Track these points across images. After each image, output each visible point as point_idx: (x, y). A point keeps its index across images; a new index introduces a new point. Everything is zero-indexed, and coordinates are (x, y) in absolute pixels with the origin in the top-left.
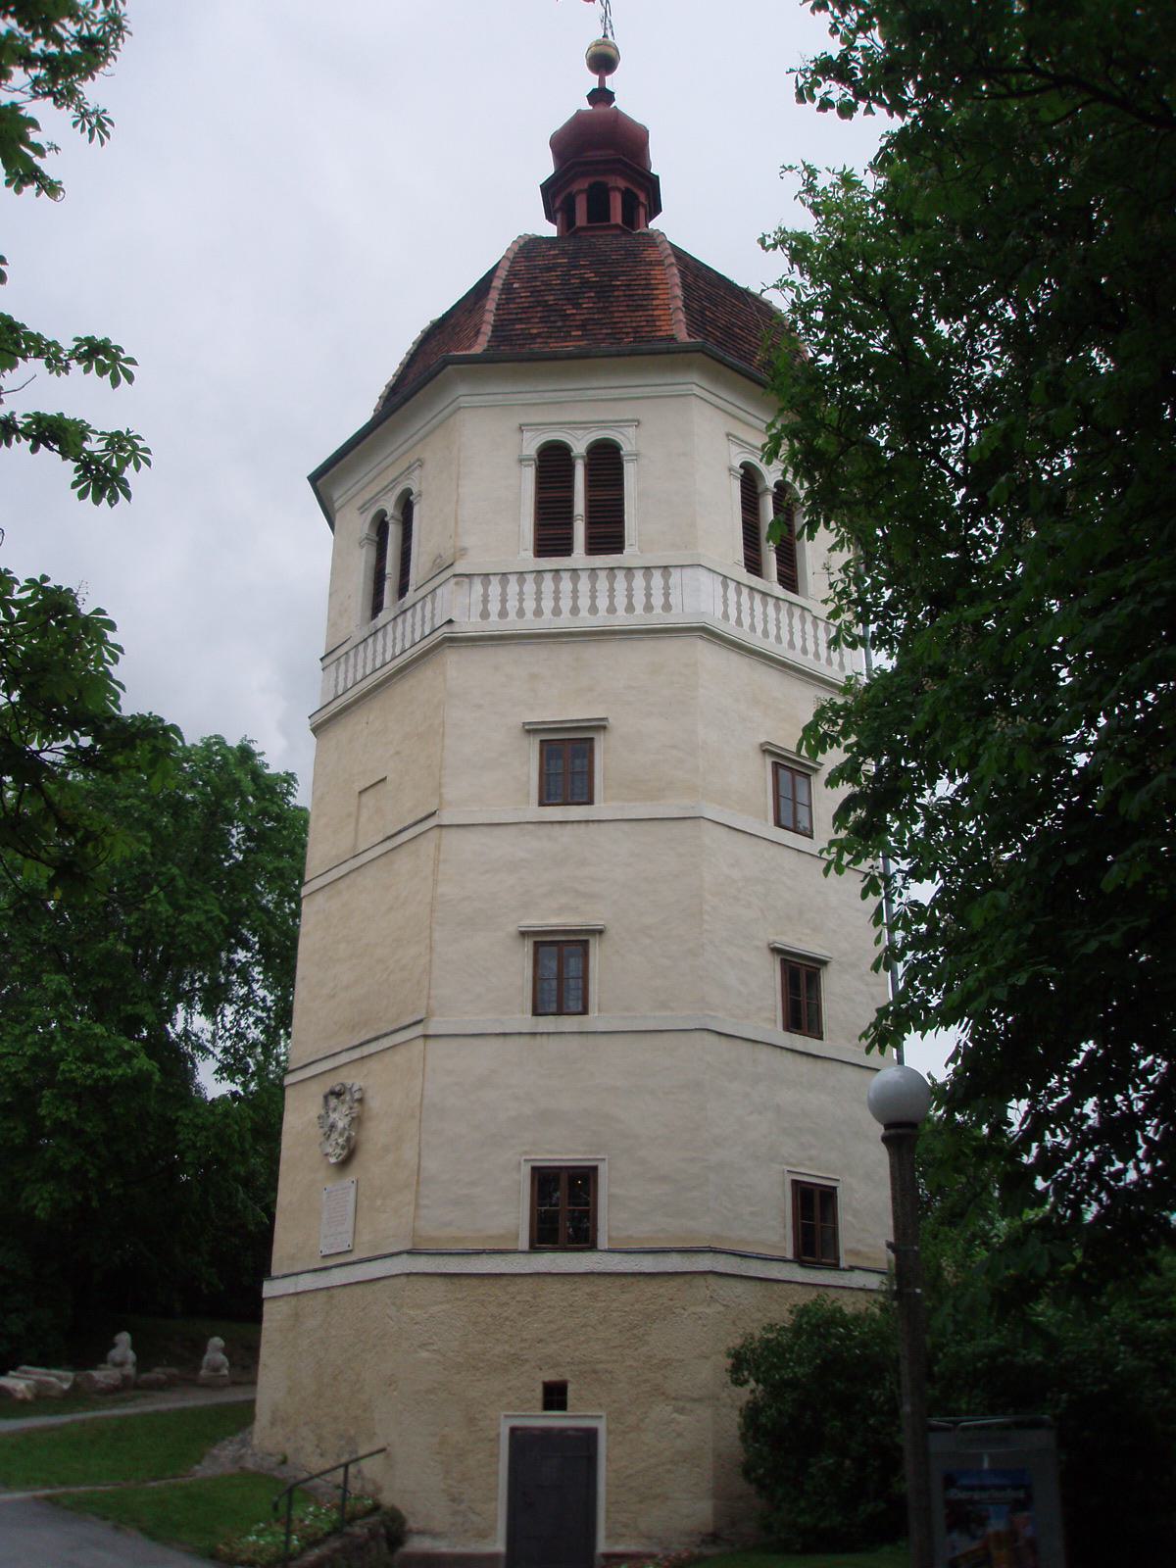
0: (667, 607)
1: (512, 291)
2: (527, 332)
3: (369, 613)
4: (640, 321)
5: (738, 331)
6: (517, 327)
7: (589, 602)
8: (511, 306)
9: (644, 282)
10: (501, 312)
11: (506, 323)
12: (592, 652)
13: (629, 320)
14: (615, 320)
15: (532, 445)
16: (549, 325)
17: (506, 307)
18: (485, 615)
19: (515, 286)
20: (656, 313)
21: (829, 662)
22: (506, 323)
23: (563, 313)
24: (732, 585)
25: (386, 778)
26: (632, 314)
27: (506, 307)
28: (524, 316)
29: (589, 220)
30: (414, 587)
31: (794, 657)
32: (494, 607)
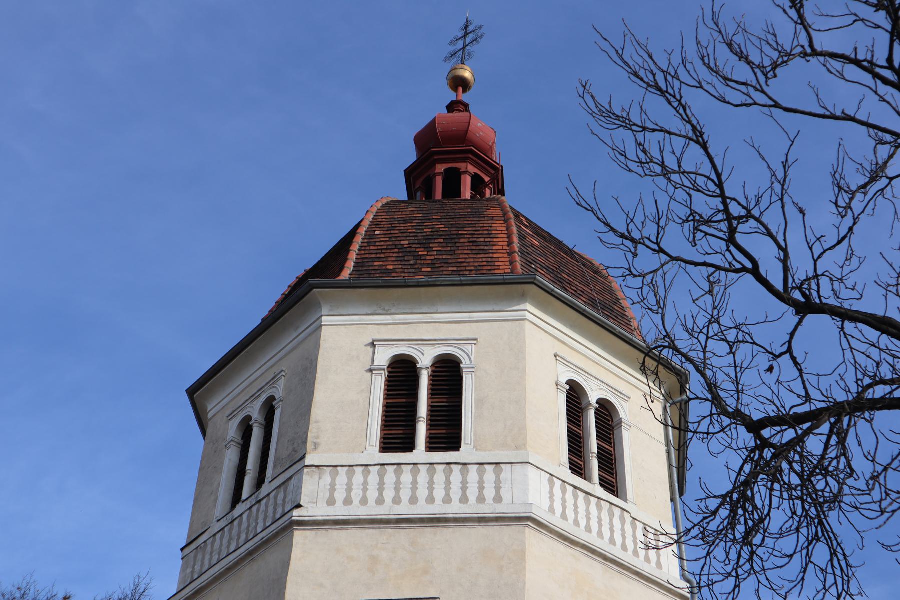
0: (498, 499)
1: (375, 237)
2: (384, 268)
3: (229, 506)
4: (482, 262)
5: (566, 277)
6: (376, 264)
8: (372, 248)
9: (486, 232)
10: (363, 252)
11: (366, 261)
12: (428, 535)
13: (472, 260)
14: (460, 261)
15: (383, 357)
16: (404, 263)
17: (368, 248)
18: (331, 502)
19: (377, 233)
20: (495, 256)
21: (647, 559)
22: (366, 261)
23: (416, 254)
24: (558, 483)
26: (475, 257)
27: (368, 248)
28: (382, 256)
29: (443, 197)
31: (616, 552)
32: (340, 496)
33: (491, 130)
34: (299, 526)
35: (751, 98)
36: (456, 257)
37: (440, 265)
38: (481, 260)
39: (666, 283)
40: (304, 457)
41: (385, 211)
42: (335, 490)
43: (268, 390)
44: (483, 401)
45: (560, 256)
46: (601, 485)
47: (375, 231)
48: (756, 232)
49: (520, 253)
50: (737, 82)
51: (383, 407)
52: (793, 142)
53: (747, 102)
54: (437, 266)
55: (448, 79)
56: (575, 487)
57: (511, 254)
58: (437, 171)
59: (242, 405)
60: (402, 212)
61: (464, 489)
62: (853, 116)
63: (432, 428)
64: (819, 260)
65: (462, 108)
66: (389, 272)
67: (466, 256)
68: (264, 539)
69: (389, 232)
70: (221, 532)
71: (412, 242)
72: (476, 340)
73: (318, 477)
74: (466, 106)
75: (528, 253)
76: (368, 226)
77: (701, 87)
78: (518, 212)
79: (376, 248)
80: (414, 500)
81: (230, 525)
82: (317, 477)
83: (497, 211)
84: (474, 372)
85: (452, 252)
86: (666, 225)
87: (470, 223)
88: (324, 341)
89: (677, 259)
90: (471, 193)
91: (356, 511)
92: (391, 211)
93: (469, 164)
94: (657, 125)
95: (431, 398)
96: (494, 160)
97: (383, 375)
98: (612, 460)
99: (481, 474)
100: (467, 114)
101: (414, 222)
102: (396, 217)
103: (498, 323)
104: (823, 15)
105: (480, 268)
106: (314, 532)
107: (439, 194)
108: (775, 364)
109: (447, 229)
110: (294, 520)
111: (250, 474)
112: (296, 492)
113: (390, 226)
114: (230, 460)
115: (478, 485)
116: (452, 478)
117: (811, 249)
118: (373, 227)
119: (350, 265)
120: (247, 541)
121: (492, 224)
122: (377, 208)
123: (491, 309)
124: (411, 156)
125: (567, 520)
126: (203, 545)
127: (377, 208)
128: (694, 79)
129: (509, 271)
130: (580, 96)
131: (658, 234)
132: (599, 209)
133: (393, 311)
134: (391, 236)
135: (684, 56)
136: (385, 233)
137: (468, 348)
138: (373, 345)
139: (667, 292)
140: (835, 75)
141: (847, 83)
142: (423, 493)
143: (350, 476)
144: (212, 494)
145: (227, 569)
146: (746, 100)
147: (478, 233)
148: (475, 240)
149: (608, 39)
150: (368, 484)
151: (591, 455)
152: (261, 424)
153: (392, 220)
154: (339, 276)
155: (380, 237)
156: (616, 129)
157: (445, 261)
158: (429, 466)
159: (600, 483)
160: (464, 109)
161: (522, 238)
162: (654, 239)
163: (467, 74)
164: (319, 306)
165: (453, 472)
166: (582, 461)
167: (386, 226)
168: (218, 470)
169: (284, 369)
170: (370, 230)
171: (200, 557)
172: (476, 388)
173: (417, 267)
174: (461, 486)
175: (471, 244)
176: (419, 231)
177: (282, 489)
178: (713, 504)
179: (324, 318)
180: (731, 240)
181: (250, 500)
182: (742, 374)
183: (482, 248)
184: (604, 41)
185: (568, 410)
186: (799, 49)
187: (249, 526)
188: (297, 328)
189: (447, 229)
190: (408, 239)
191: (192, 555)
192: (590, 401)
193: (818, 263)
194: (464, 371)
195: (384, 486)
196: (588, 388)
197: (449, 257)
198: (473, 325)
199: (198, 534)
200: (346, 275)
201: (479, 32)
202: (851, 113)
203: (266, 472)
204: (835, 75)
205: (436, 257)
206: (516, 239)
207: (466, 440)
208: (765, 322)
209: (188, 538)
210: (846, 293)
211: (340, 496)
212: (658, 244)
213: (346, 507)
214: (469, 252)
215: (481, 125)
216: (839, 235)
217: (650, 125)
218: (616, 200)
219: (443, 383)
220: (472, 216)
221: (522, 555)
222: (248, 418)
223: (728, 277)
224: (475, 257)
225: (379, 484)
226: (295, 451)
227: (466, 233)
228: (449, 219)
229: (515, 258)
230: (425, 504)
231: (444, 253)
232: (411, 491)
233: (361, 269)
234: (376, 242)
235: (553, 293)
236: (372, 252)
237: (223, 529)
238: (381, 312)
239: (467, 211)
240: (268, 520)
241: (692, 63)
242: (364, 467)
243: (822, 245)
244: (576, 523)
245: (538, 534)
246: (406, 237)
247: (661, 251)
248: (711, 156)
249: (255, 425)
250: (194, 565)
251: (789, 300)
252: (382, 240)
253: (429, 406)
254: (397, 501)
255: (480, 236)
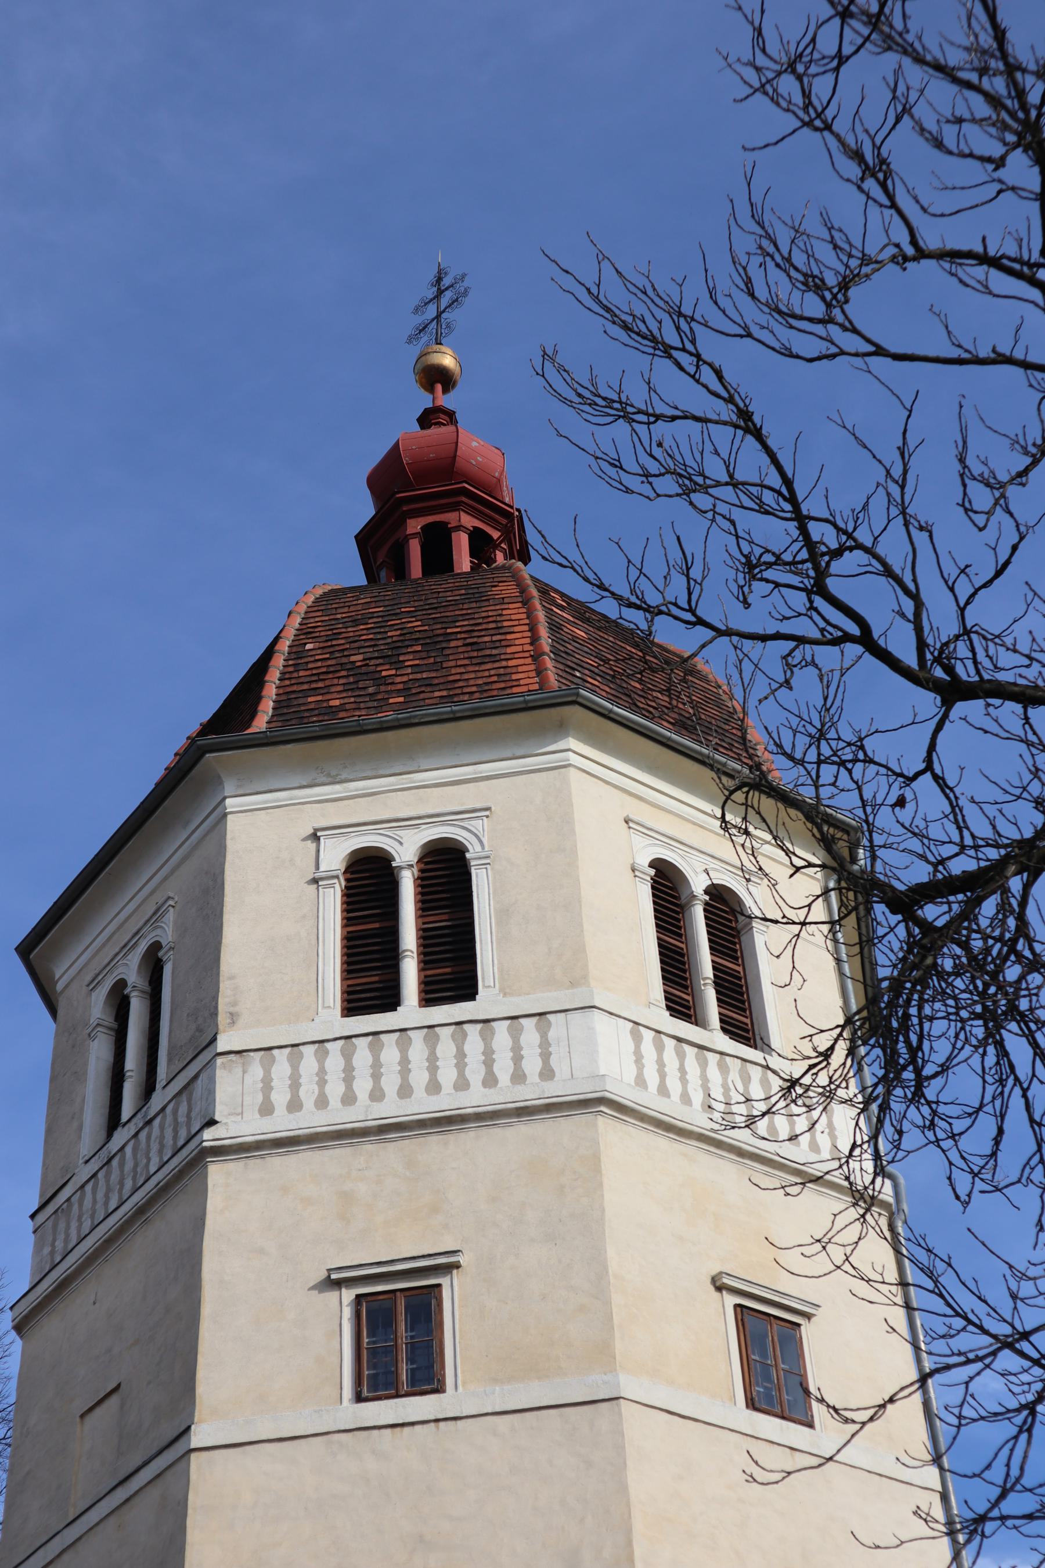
0: (547, 1073)
2: (325, 705)
3: (103, 1134)
4: (491, 676)
6: (310, 699)
7: (426, 1076)
8: (301, 673)
10: (287, 682)
11: (293, 696)
13: (473, 675)
14: (452, 678)
17: (295, 675)
18: (267, 1109)
19: (309, 647)
20: (511, 663)
22: (293, 696)
23: (377, 676)
24: (648, 1036)
25: (119, 1386)
27: (295, 675)
28: (320, 684)
30: (164, 1083)
32: (280, 1097)
33: (496, 451)
34: (215, 1157)
35: (833, 343)
36: (444, 672)
37: (418, 690)
38: (487, 674)
39: (743, 676)
40: (214, 1040)
41: (320, 608)
42: (271, 1088)
43: (149, 932)
44: (508, 910)
45: (624, 651)
46: (725, 1030)
47: (305, 644)
48: (866, 573)
49: (552, 655)
50: (810, 320)
51: (342, 939)
52: (911, 411)
53: (829, 352)
54: (414, 691)
55: (416, 371)
56: (679, 1040)
57: (537, 656)
58: (408, 532)
59: (112, 960)
60: (349, 606)
61: (489, 1062)
62: (1008, 353)
63: (428, 966)
64: (969, 607)
65: (443, 418)
66: (333, 711)
67: (462, 670)
68: (161, 1184)
69: (329, 644)
70: (93, 1180)
71: (369, 655)
72: (488, 809)
73: (241, 1069)
74: (451, 416)
75: (566, 653)
76: (292, 638)
77: (749, 335)
78: (547, 585)
79: (308, 673)
80: (405, 1091)
81: (106, 1167)
82: (238, 1070)
83: (509, 588)
84: (489, 864)
85: (438, 666)
86: (704, 578)
87: (464, 612)
88: (231, 839)
89: (729, 633)
90: (471, 562)
91: (310, 1120)
92: (330, 607)
93: (462, 513)
94: (676, 408)
95: (421, 916)
96: (507, 500)
97: (337, 886)
98: (741, 986)
99: (515, 1035)
100: (452, 428)
101: (370, 621)
102: (339, 616)
103: (524, 776)
104: (946, 188)
105: (486, 688)
106: (240, 1164)
107: (416, 569)
108: (909, 795)
109: (426, 628)
110: (206, 1147)
111: (131, 1077)
112: (207, 1099)
113: (330, 633)
114: (98, 1058)
115: (511, 1054)
116: (467, 1048)
117: (952, 589)
118: (302, 637)
119: (267, 707)
120: (136, 1190)
121: (502, 609)
122: (306, 604)
123: (509, 754)
124: (365, 510)
125: (668, 1096)
126: (66, 1204)
127: (306, 604)
128: (735, 322)
129: (537, 686)
130: (537, 374)
131: (690, 594)
132: (586, 563)
133: (343, 777)
134: (331, 650)
135: (711, 286)
136: (322, 645)
137: (477, 825)
138: (315, 837)
139: (747, 691)
140: (973, 288)
141: (995, 299)
142: (419, 1078)
143: (295, 1063)
144: (73, 1118)
145: (105, 1241)
146: (828, 349)
147: (480, 628)
148: (475, 640)
149: (570, 271)
150: (326, 1073)
151: (702, 982)
152: (142, 992)
153: (333, 622)
154: (249, 726)
155: (314, 653)
156: (611, 423)
157: (427, 682)
158: (426, 1030)
159: (722, 1028)
160: (448, 420)
161: (555, 627)
162: (683, 602)
163: (448, 361)
164: (219, 782)
165: (468, 1037)
166: (688, 994)
167: (322, 634)
168: (80, 1076)
169: (171, 895)
170: (297, 643)
171: (62, 1225)
172: (495, 891)
173: (379, 697)
174: (483, 1058)
175: (469, 648)
176: (379, 636)
177: (184, 1097)
178: (823, 1042)
179: (228, 801)
180: (819, 588)
181: (134, 1121)
182: (875, 815)
183: (488, 652)
184: (565, 273)
185: (655, 910)
186: (892, 250)
187: (136, 1165)
188: (187, 823)
189: (426, 628)
190: (361, 651)
191: (50, 1223)
192: (693, 892)
193: (967, 612)
194: (472, 864)
195: (354, 1073)
196: (687, 868)
197: (434, 674)
198: (482, 784)
199: (57, 1188)
200: (261, 723)
201: (461, 287)
202: (1005, 349)
203: (156, 1073)
204: (973, 288)
205: (411, 677)
206: (544, 632)
207: (486, 981)
208: (913, 723)
209: (41, 1196)
210: (1006, 659)
211: (280, 1097)
212: (691, 611)
213: (292, 1116)
214: (466, 662)
215: (477, 444)
216: (997, 561)
217: (661, 409)
218: (617, 543)
219: (440, 889)
220: (467, 601)
221: (594, 1163)
222: (121, 984)
223: (845, 654)
224: (477, 669)
225: (344, 1071)
226: (200, 1030)
227: (458, 630)
228: (429, 609)
229: (544, 663)
230: (425, 1095)
231: (424, 668)
232: (399, 1076)
233: (285, 711)
234: (307, 663)
235: (612, 715)
236: (301, 680)
237: (94, 1175)
238: (324, 779)
239: (457, 592)
240: (165, 1151)
241: (730, 296)
242: (317, 1045)
243: (971, 581)
244: (686, 1099)
245: (619, 1125)
246: (359, 648)
247: (701, 622)
248: (772, 451)
249: (133, 994)
250: (54, 1240)
251: (927, 681)
252: (317, 657)
253: (418, 930)
254: (377, 1095)
255: (483, 633)
